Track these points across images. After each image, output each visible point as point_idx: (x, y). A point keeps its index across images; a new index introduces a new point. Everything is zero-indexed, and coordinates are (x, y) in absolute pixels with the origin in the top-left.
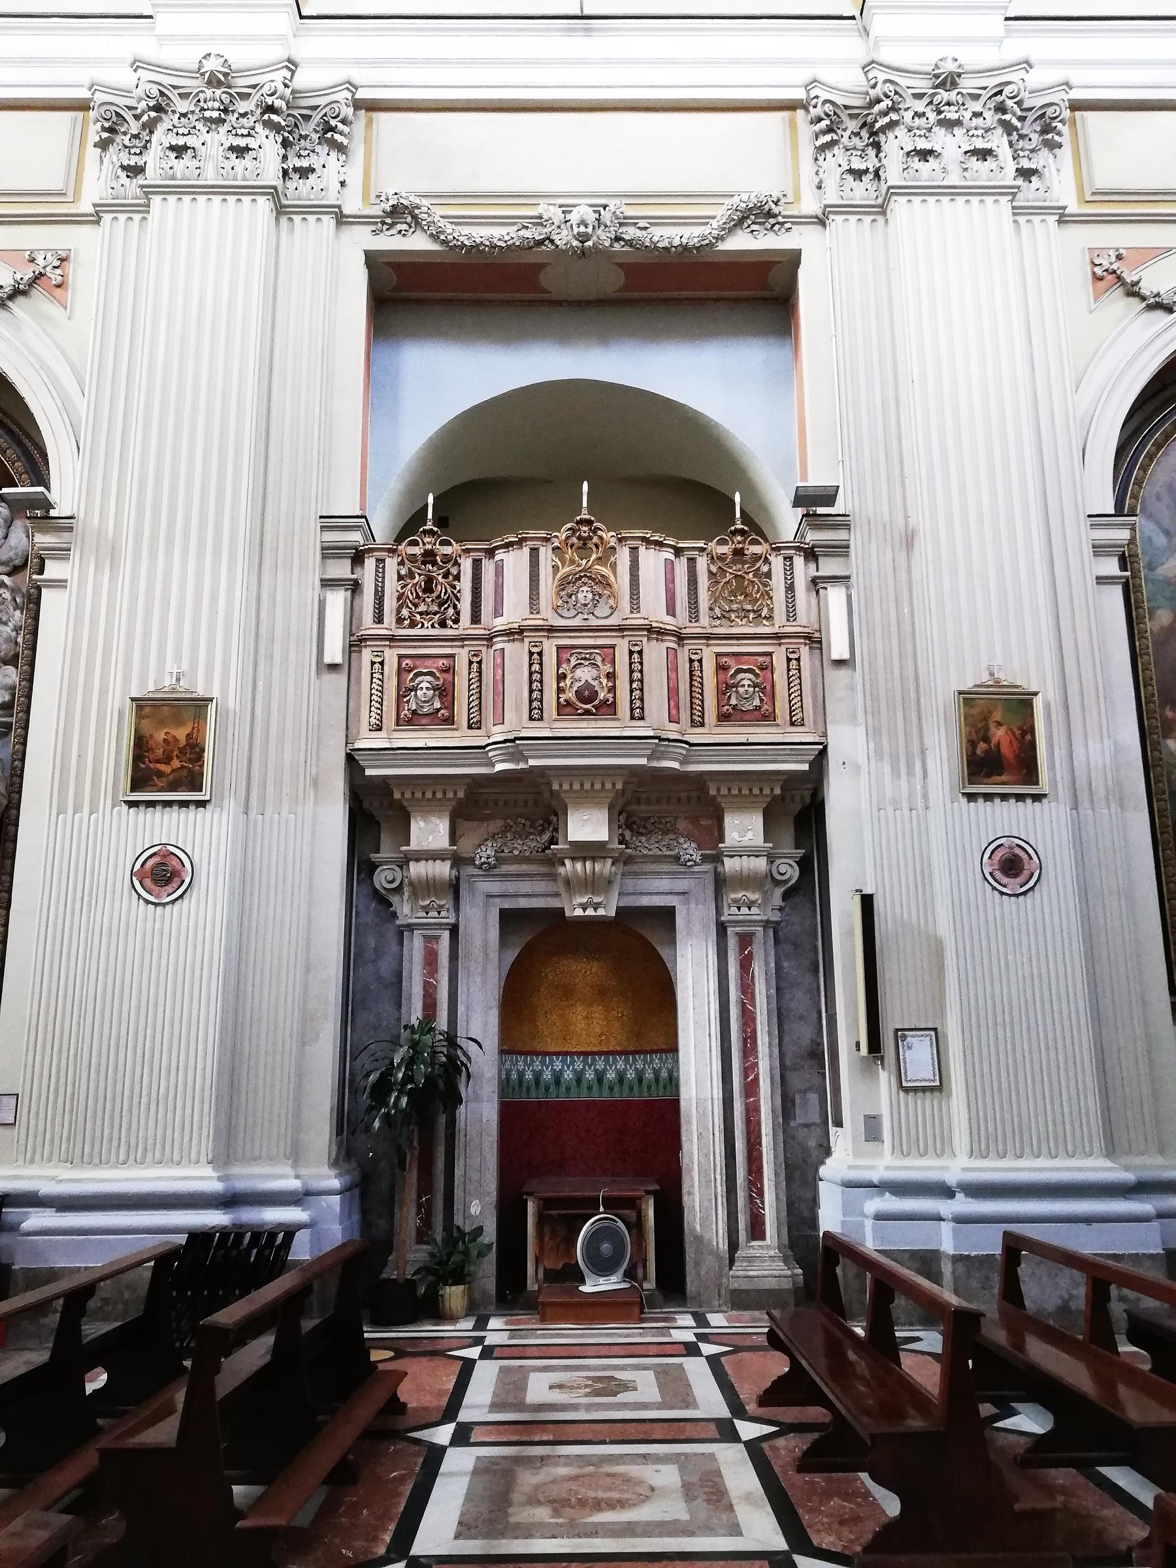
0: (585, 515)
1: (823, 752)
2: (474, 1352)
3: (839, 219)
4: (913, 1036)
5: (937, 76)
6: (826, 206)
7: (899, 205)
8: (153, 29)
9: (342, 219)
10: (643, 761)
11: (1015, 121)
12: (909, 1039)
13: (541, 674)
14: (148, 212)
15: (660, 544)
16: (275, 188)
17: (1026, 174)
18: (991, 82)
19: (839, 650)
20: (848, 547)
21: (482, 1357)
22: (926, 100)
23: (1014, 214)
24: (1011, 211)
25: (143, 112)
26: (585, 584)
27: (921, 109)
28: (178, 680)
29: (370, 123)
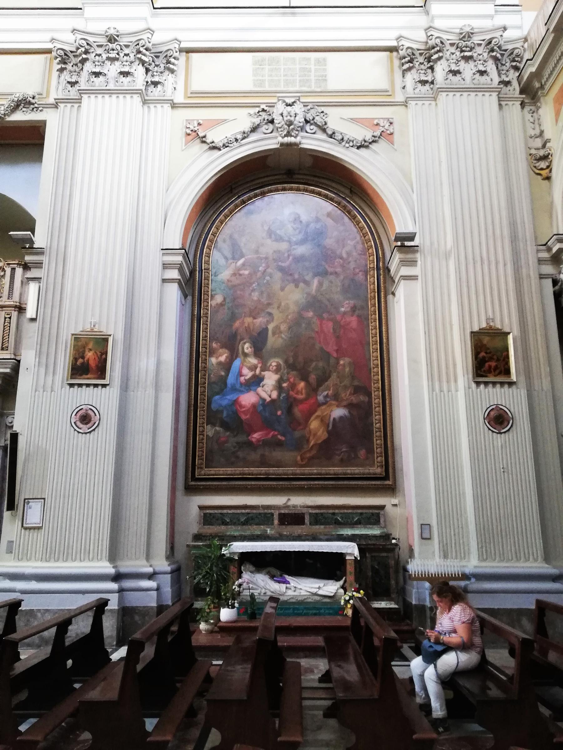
3: (413, 103)
4: (33, 502)
6: (407, 98)
8: (83, 15)
11: (498, 55)
12: (30, 504)
14: (81, 103)
16: (141, 90)
18: (488, 37)
19: (30, 312)
20: (42, 263)
25: (80, 55)
27: (453, 51)
28: (94, 326)
29: (188, 59)
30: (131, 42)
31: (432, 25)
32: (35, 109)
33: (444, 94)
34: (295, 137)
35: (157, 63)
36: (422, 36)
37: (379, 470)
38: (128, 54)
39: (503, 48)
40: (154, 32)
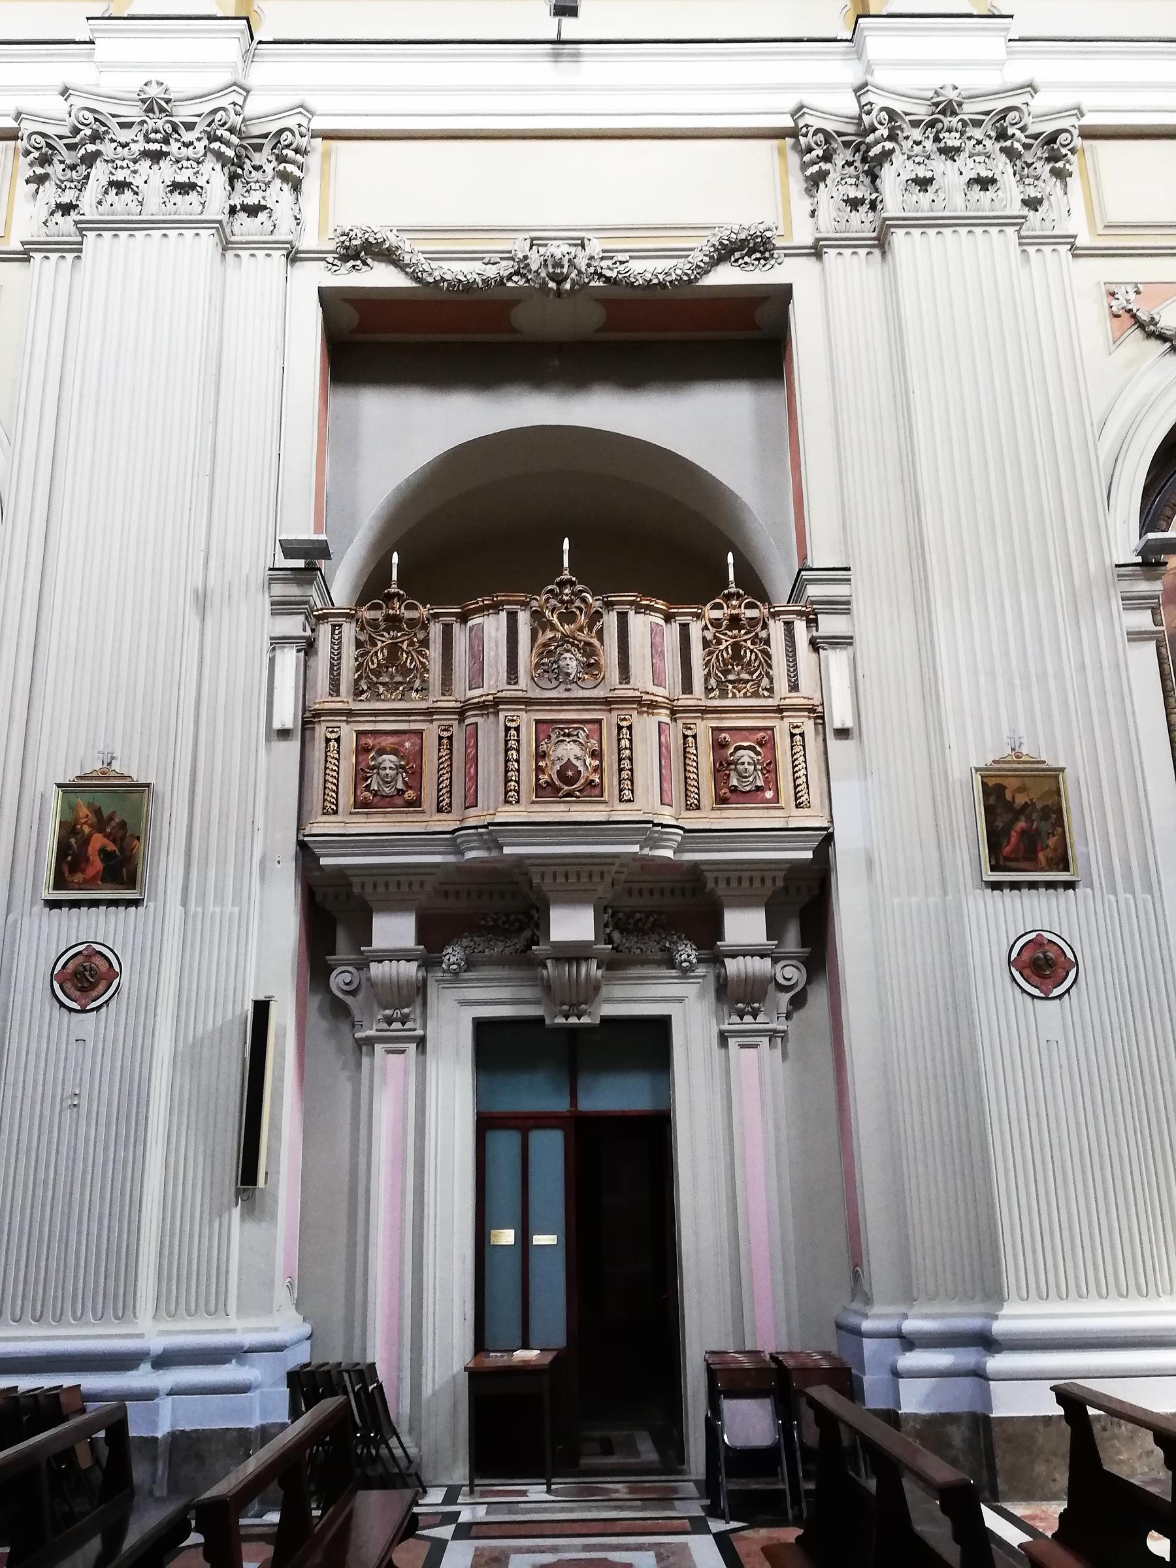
0: (566, 575)
1: (829, 839)
2: (446, 1532)
7: (898, 237)
8: (92, 55)
9: (294, 256)
10: (635, 848)
13: (631, 749)
14: (81, 250)
15: (649, 608)
16: (220, 222)
17: (1033, 204)
21: (456, 1537)
22: (135, 128)
23: (1020, 244)
26: (568, 651)
29: (326, 156)
32: (763, 262)
33: (900, 232)
35: (257, 163)
38: (191, 143)
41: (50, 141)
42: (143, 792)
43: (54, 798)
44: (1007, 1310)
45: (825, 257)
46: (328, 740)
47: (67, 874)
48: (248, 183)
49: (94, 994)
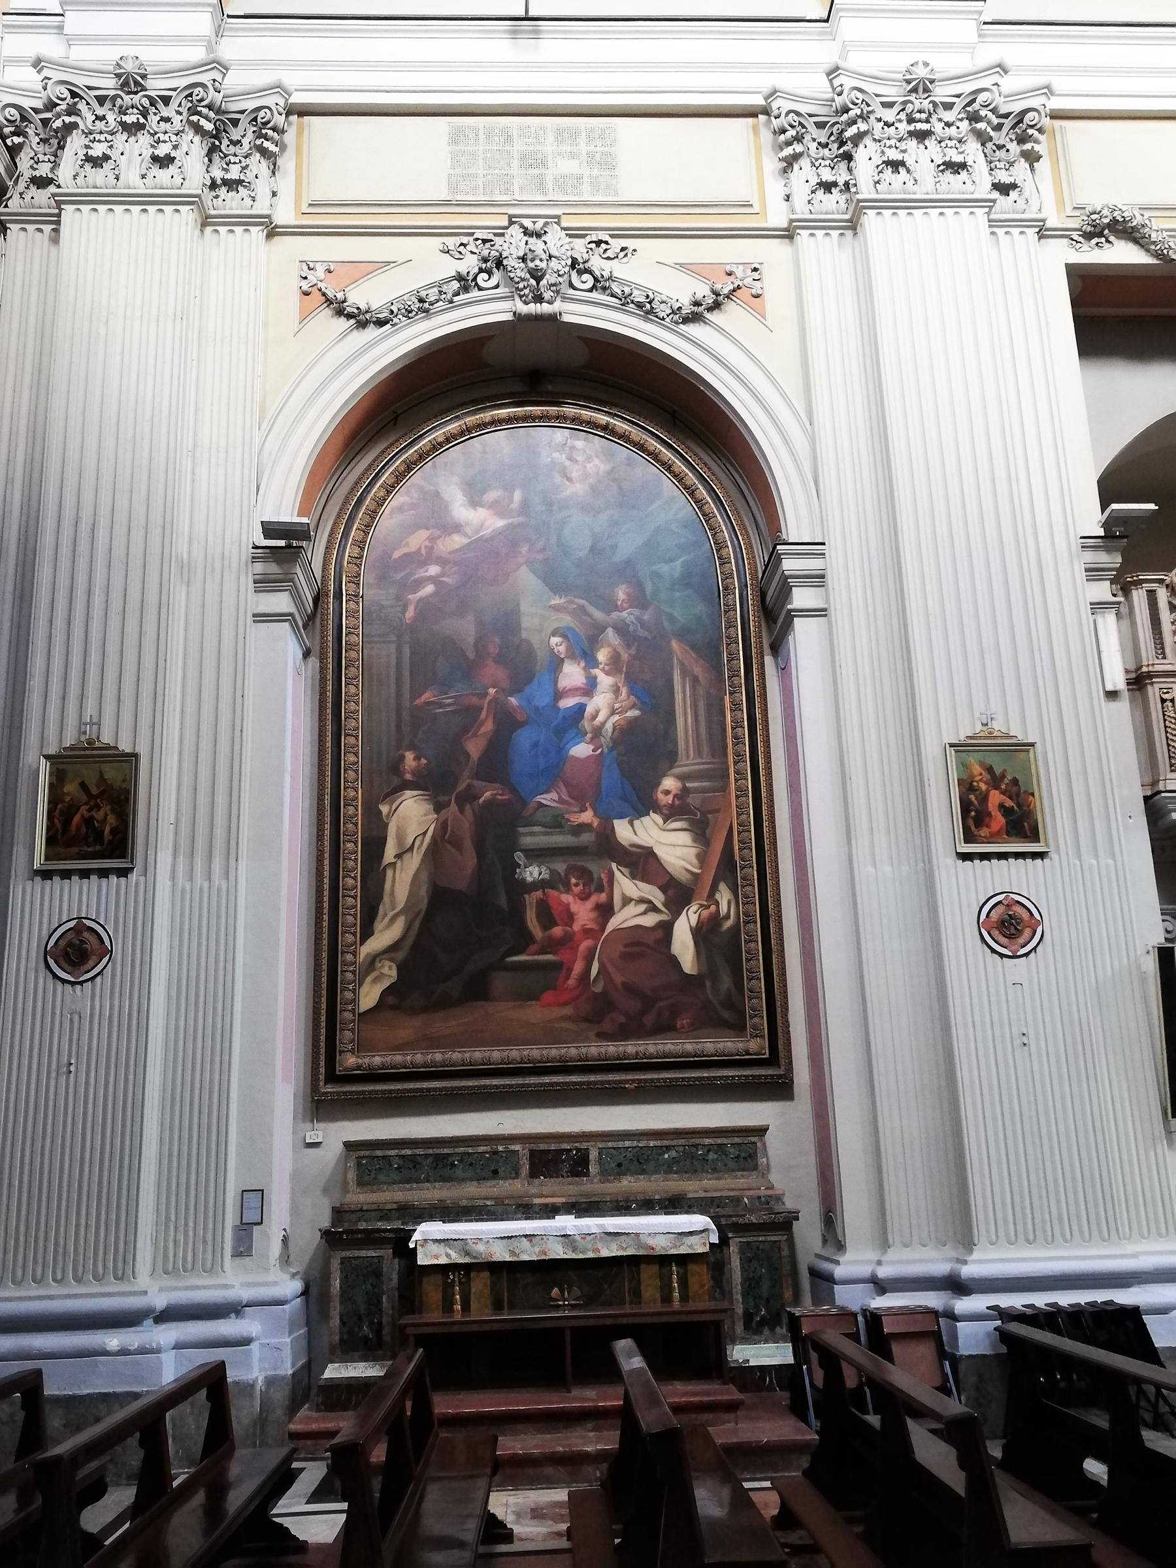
3: (805, 233)
5: (908, 82)
6: (792, 221)
7: (870, 218)
9: (273, 232)
14: (58, 223)
17: (1004, 189)
22: (897, 108)
23: (990, 226)
24: (987, 223)
30: (174, 90)
31: (841, 64)
34: (550, 303)
36: (820, 86)
37: (753, 1045)
39: (1003, 111)
40: (227, 69)
41: (802, 121)
42: (1028, 751)
43: (44, 768)
44: (976, 1255)
45: (798, 239)
46: (1163, 701)
47: (973, 828)
48: (226, 156)
49: (1021, 941)
